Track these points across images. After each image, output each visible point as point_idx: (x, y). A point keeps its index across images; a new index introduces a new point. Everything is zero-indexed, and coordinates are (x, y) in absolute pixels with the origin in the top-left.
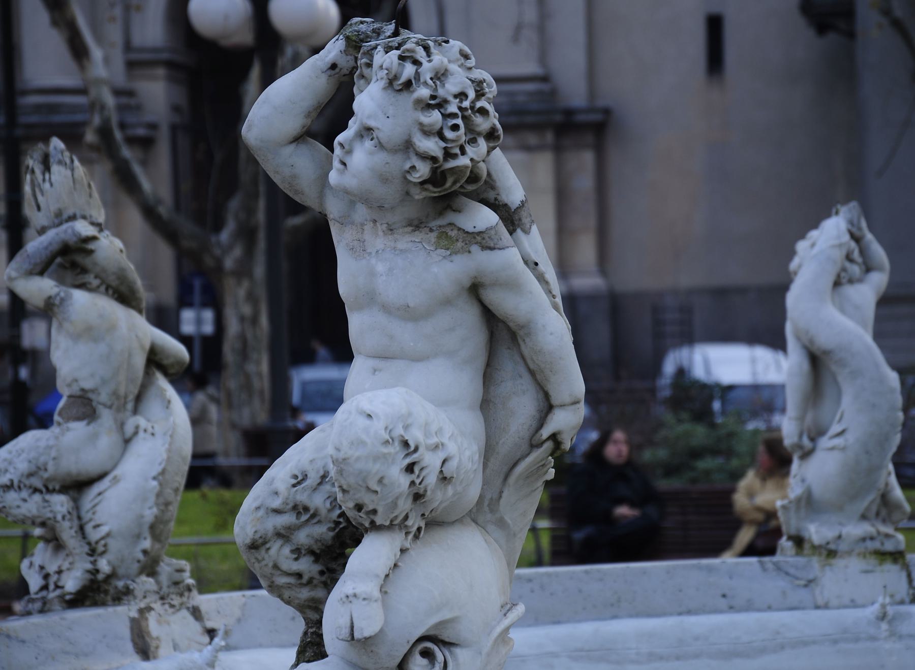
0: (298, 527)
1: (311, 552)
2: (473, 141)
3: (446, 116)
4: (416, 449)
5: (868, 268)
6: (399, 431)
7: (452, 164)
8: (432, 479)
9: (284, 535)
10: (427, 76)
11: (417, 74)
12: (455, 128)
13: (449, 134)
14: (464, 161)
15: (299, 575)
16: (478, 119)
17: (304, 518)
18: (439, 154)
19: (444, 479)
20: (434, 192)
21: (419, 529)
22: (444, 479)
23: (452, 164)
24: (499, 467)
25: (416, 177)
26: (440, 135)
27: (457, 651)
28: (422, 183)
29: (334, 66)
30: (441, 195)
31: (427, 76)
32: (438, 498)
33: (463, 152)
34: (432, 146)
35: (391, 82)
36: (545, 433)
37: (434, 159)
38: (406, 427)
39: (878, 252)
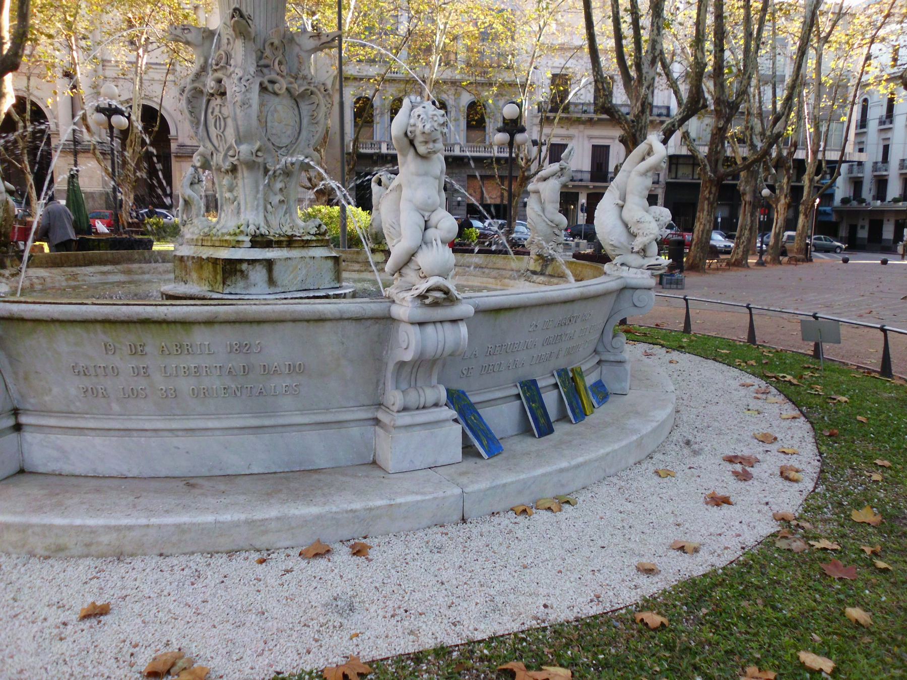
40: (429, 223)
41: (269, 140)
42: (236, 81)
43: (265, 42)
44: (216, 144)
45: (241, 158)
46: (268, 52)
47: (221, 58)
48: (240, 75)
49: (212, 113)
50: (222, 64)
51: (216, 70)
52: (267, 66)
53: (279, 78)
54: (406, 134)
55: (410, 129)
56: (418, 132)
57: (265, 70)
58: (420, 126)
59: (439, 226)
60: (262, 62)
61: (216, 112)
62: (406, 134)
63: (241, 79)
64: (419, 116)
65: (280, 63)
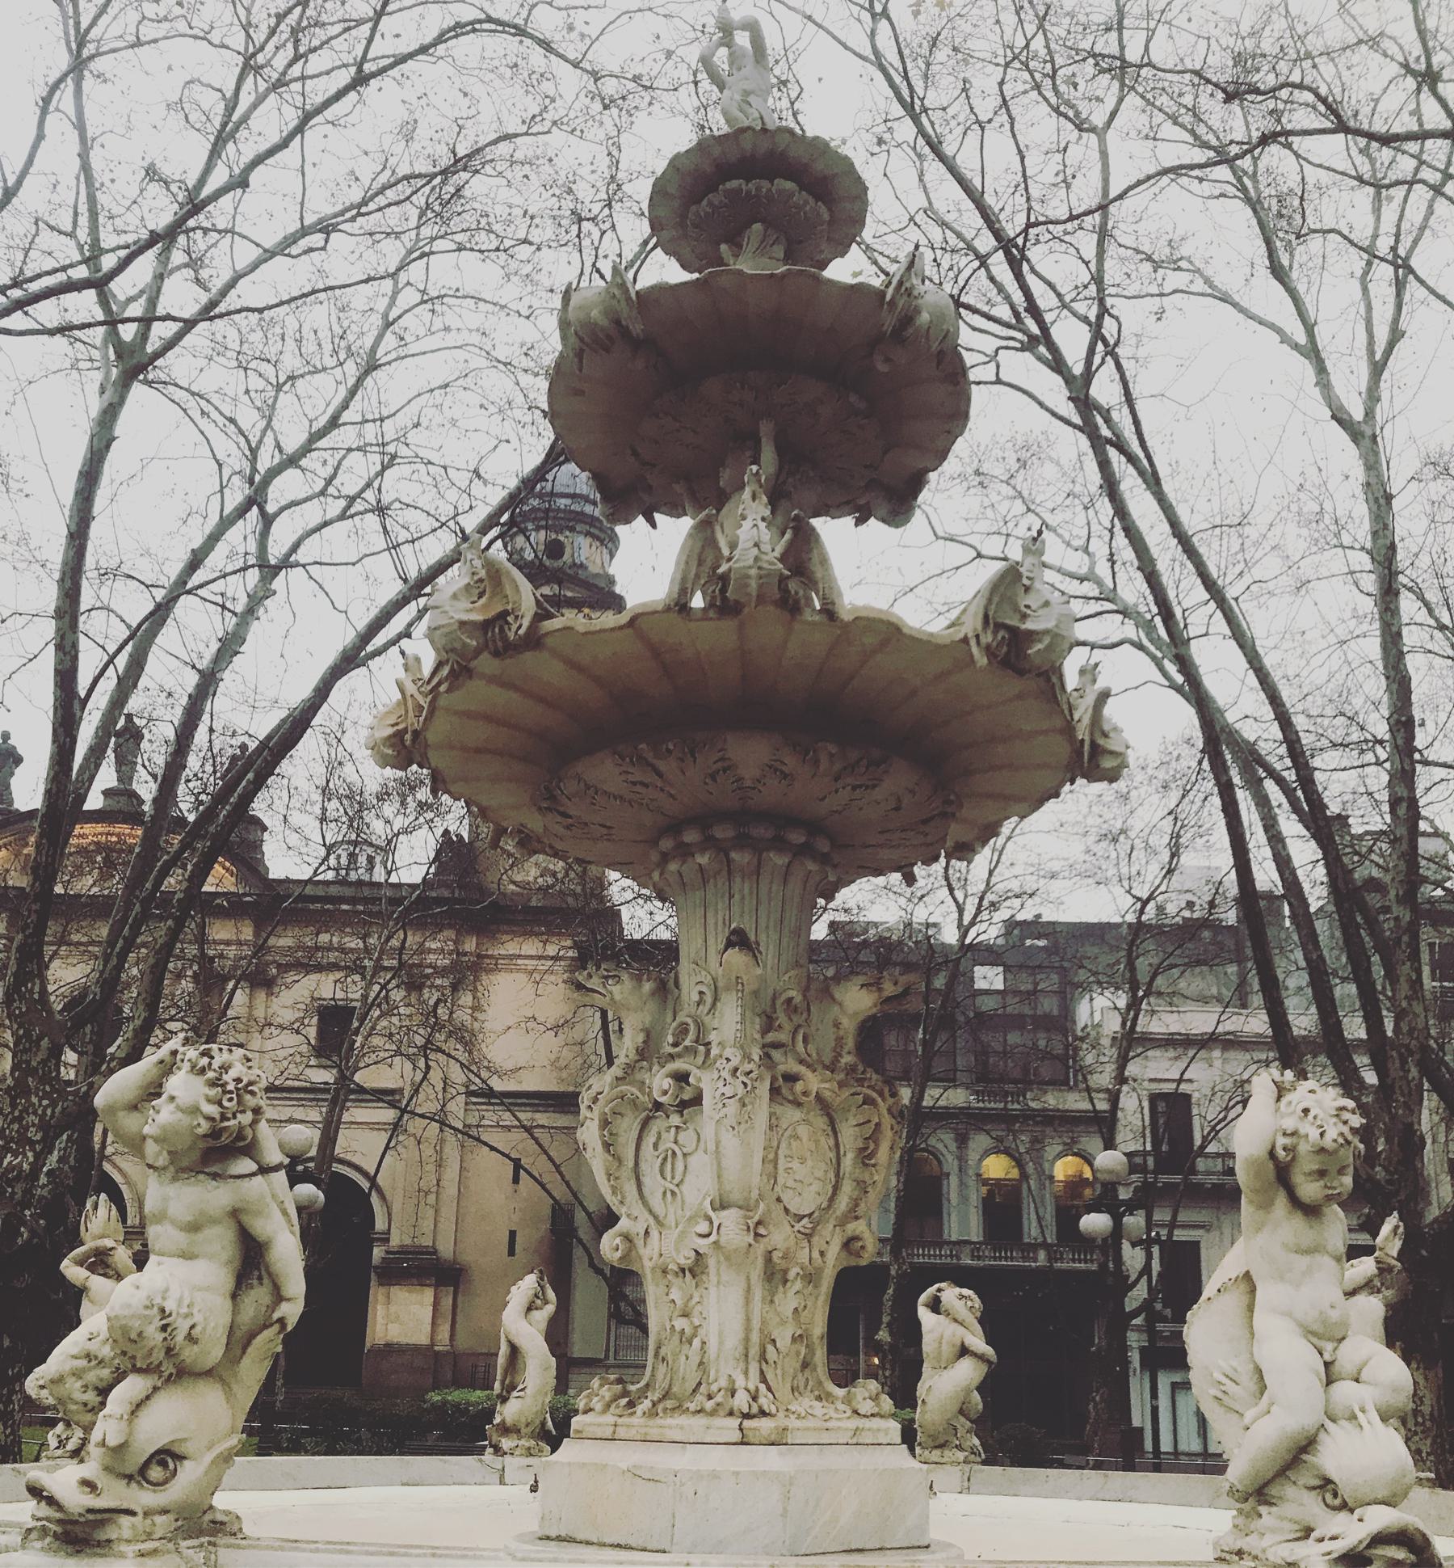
0: (90, 1369)
1: (97, 1388)
2: (243, 1112)
3: (225, 1092)
4: (170, 1315)
5: (547, 1303)
6: (158, 1300)
7: (226, 1124)
8: (180, 1337)
9: (77, 1374)
10: (215, 1065)
11: (210, 1064)
12: (230, 1100)
13: (226, 1103)
14: (232, 1123)
15: (85, 1405)
16: (248, 1097)
17: (94, 1363)
18: (218, 1117)
19: (191, 1339)
20: (211, 1143)
21: (171, 1375)
22: (191, 1339)
23: (226, 1124)
24: (239, 1342)
25: (200, 1131)
26: (220, 1104)
27: (186, 1462)
28: (205, 1136)
29: (162, 1062)
30: (217, 1150)
31: (215, 1065)
32: (189, 1354)
33: (235, 1117)
34: (212, 1110)
35: (193, 1067)
36: (276, 1316)
37: (213, 1119)
38: (164, 1299)
39: (551, 1294)
40: (1336, 1368)
41: (779, 1200)
42: (725, 1074)
43: (774, 999)
44: (659, 1209)
45: (723, 1241)
46: (782, 1018)
47: (686, 1031)
48: (735, 1062)
49: (656, 1146)
50: (687, 1043)
51: (672, 1057)
52: (777, 1046)
53: (802, 1069)
54: (1272, 1154)
55: (1281, 1141)
56: (1303, 1148)
57: (777, 1055)
58: (1314, 1134)
59: (1363, 1376)
60: (771, 1037)
61: (667, 1143)
62: (1272, 1154)
63: (736, 1070)
64: (1306, 1111)
65: (805, 1040)
